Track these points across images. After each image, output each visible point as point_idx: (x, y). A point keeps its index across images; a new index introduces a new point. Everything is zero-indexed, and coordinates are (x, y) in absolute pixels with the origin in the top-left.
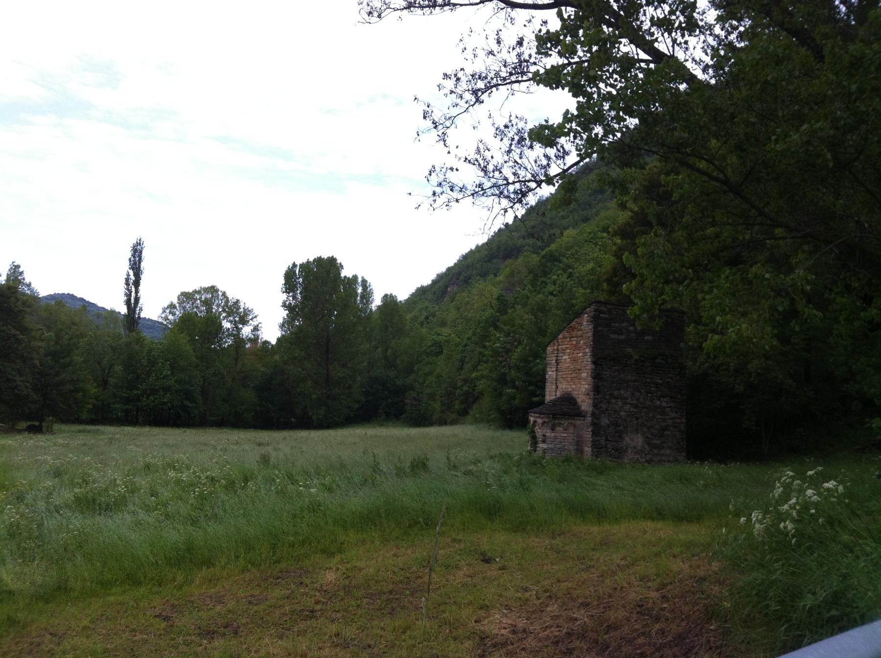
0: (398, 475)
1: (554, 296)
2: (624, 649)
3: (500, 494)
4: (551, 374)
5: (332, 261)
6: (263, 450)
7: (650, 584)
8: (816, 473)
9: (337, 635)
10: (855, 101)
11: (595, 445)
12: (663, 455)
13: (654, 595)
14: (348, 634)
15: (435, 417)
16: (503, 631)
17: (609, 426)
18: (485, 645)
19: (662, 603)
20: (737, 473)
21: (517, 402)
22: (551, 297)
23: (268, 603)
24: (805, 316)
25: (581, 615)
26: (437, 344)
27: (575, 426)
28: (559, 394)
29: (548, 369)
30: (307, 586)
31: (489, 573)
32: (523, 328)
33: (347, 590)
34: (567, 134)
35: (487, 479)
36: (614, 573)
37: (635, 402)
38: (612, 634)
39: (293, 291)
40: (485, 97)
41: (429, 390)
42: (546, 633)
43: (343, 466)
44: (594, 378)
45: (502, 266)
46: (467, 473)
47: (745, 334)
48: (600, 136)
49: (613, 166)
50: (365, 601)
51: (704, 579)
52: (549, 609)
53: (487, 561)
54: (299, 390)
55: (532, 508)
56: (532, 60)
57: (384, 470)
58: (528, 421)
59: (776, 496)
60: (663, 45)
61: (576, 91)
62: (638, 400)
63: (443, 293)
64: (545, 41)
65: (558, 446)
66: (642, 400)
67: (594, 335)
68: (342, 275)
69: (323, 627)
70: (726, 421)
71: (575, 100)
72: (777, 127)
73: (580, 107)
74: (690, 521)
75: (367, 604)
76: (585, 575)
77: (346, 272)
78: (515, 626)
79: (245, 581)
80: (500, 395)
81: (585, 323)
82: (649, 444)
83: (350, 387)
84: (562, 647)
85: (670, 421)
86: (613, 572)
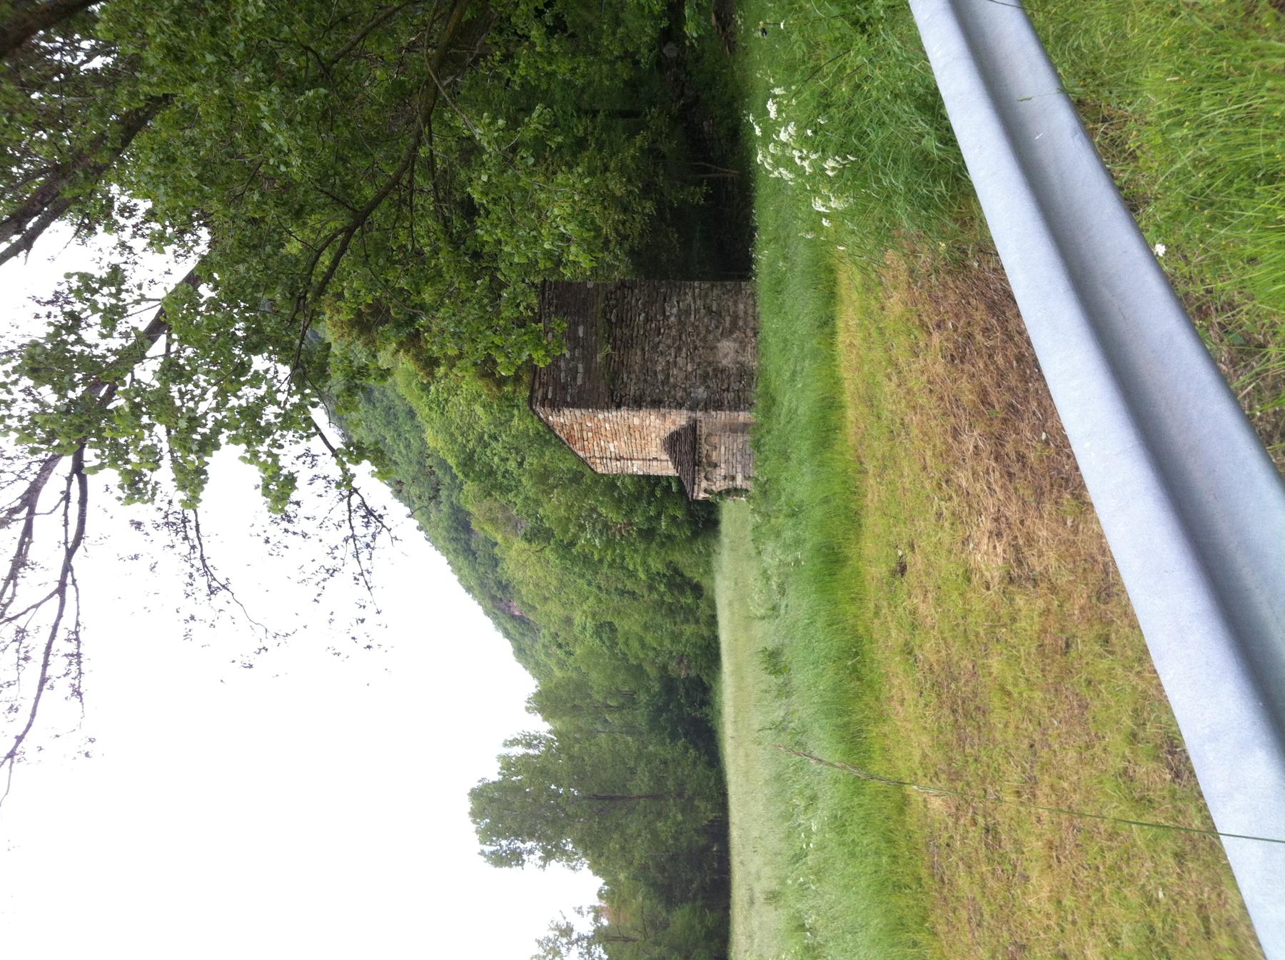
0: (788, 695)
1: (523, 459)
2: (1013, 383)
3: (808, 545)
4: (636, 468)
5: (476, 795)
6: (759, 897)
7: (922, 344)
8: (758, 124)
9: (1018, 794)
10: (230, 57)
11: (736, 406)
12: (746, 313)
13: (936, 338)
14: (1016, 777)
15: (706, 633)
16: (999, 550)
17: (708, 387)
18: (1020, 577)
19: (946, 329)
20: (766, 215)
21: (679, 514)
22: (526, 465)
23: (978, 897)
24: (541, 128)
25: (970, 441)
26: (598, 631)
27: (709, 435)
28: (665, 457)
29: (630, 471)
30: (951, 837)
31: (919, 566)
32: (572, 505)
33: (954, 776)
34: (276, 458)
35: (789, 564)
36: (909, 391)
37: (673, 351)
38: (994, 399)
39: (521, 854)
40: (220, 577)
41: (667, 642)
42: (997, 489)
43: (778, 778)
44: (640, 407)
45: (482, 534)
46: (782, 591)
47: (569, 210)
48: (279, 411)
49: (325, 389)
50: (968, 750)
51: (911, 271)
52: (964, 484)
53: (903, 569)
54: (671, 842)
55: (826, 501)
56: (165, 506)
57: (782, 714)
58: (706, 501)
59: (791, 176)
60: (141, 318)
61: (209, 445)
63: (523, 622)
64: (135, 487)
65: (739, 458)
66: (669, 341)
67: (579, 407)
68: (497, 778)
69: (1008, 814)
70: (700, 223)
71: (223, 447)
72: (268, 164)
73: (234, 440)
74: (835, 282)
75: (972, 746)
76: (915, 432)
78: (991, 533)
79: (949, 932)
80: (670, 537)
81: (563, 419)
82: (731, 332)
83: (665, 763)
84: (1015, 468)
85: (698, 302)
86: (908, 393)
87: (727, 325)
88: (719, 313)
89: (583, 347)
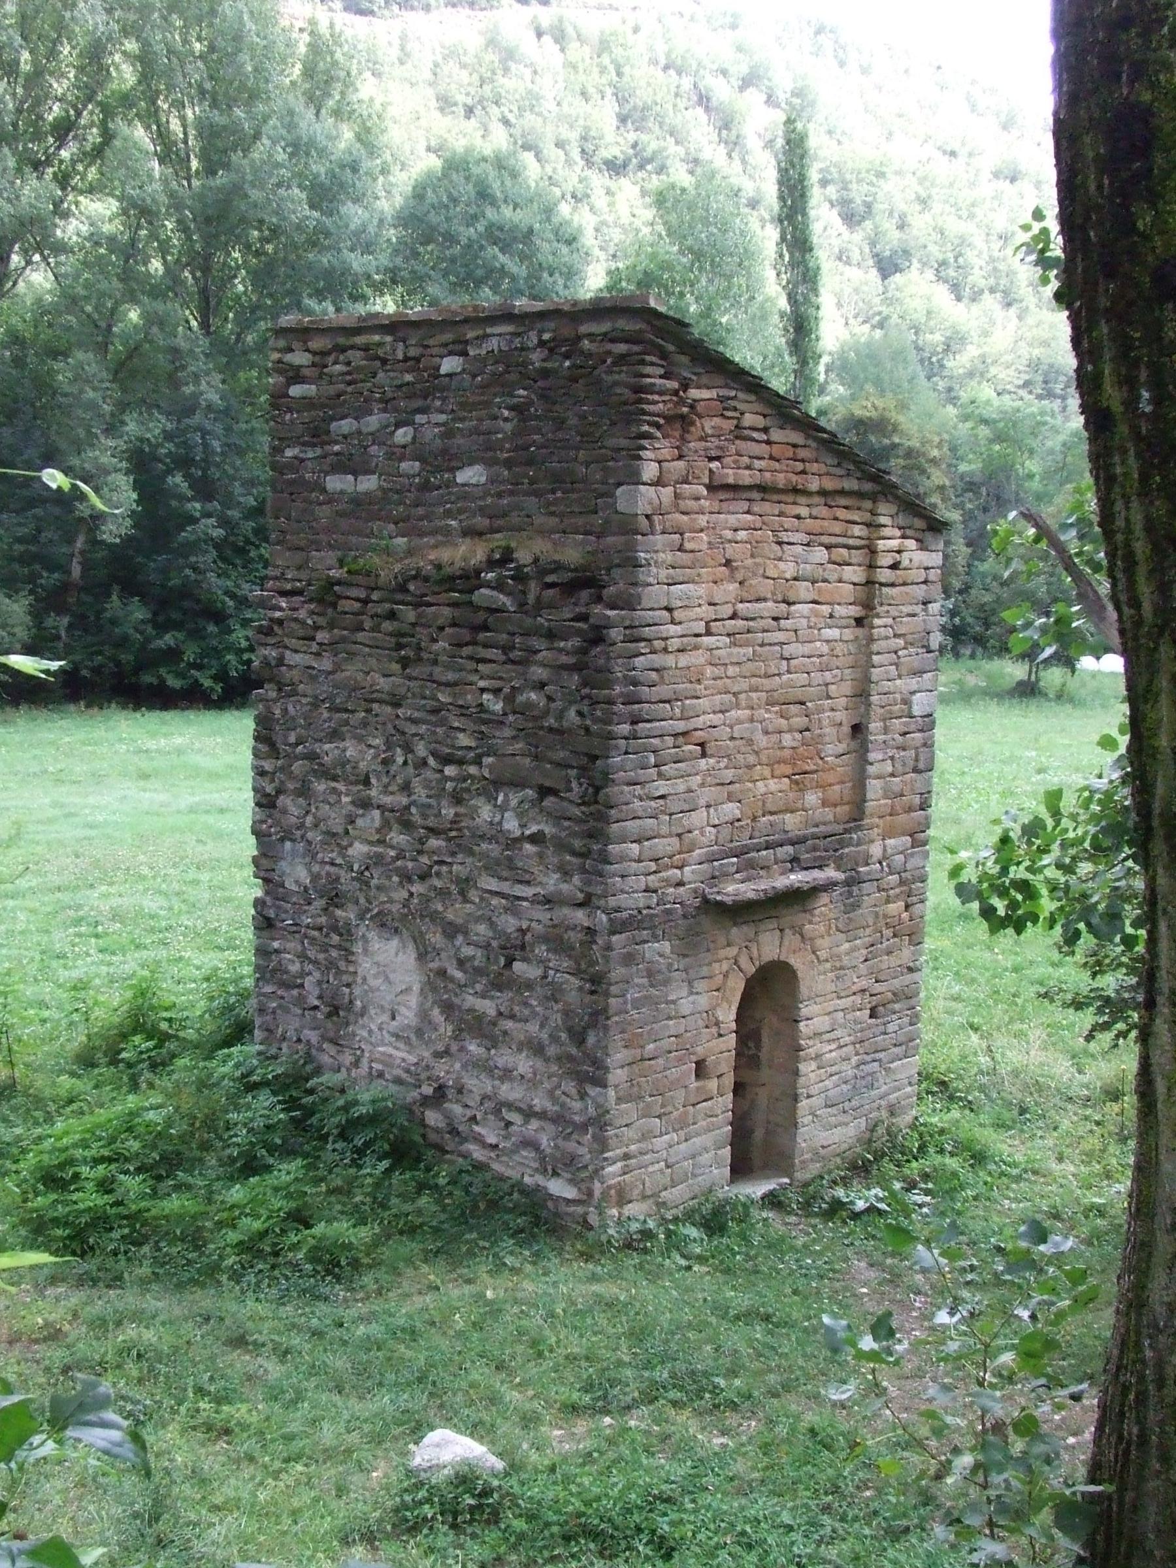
12: (507, 1074)
62: (406, 788)
66: (420, 793)
77: (96, 709)
82: (448, 1008)
85: (542, 914)
87: (470, 1001)
88: (499, 984)
89: (425, 487)
